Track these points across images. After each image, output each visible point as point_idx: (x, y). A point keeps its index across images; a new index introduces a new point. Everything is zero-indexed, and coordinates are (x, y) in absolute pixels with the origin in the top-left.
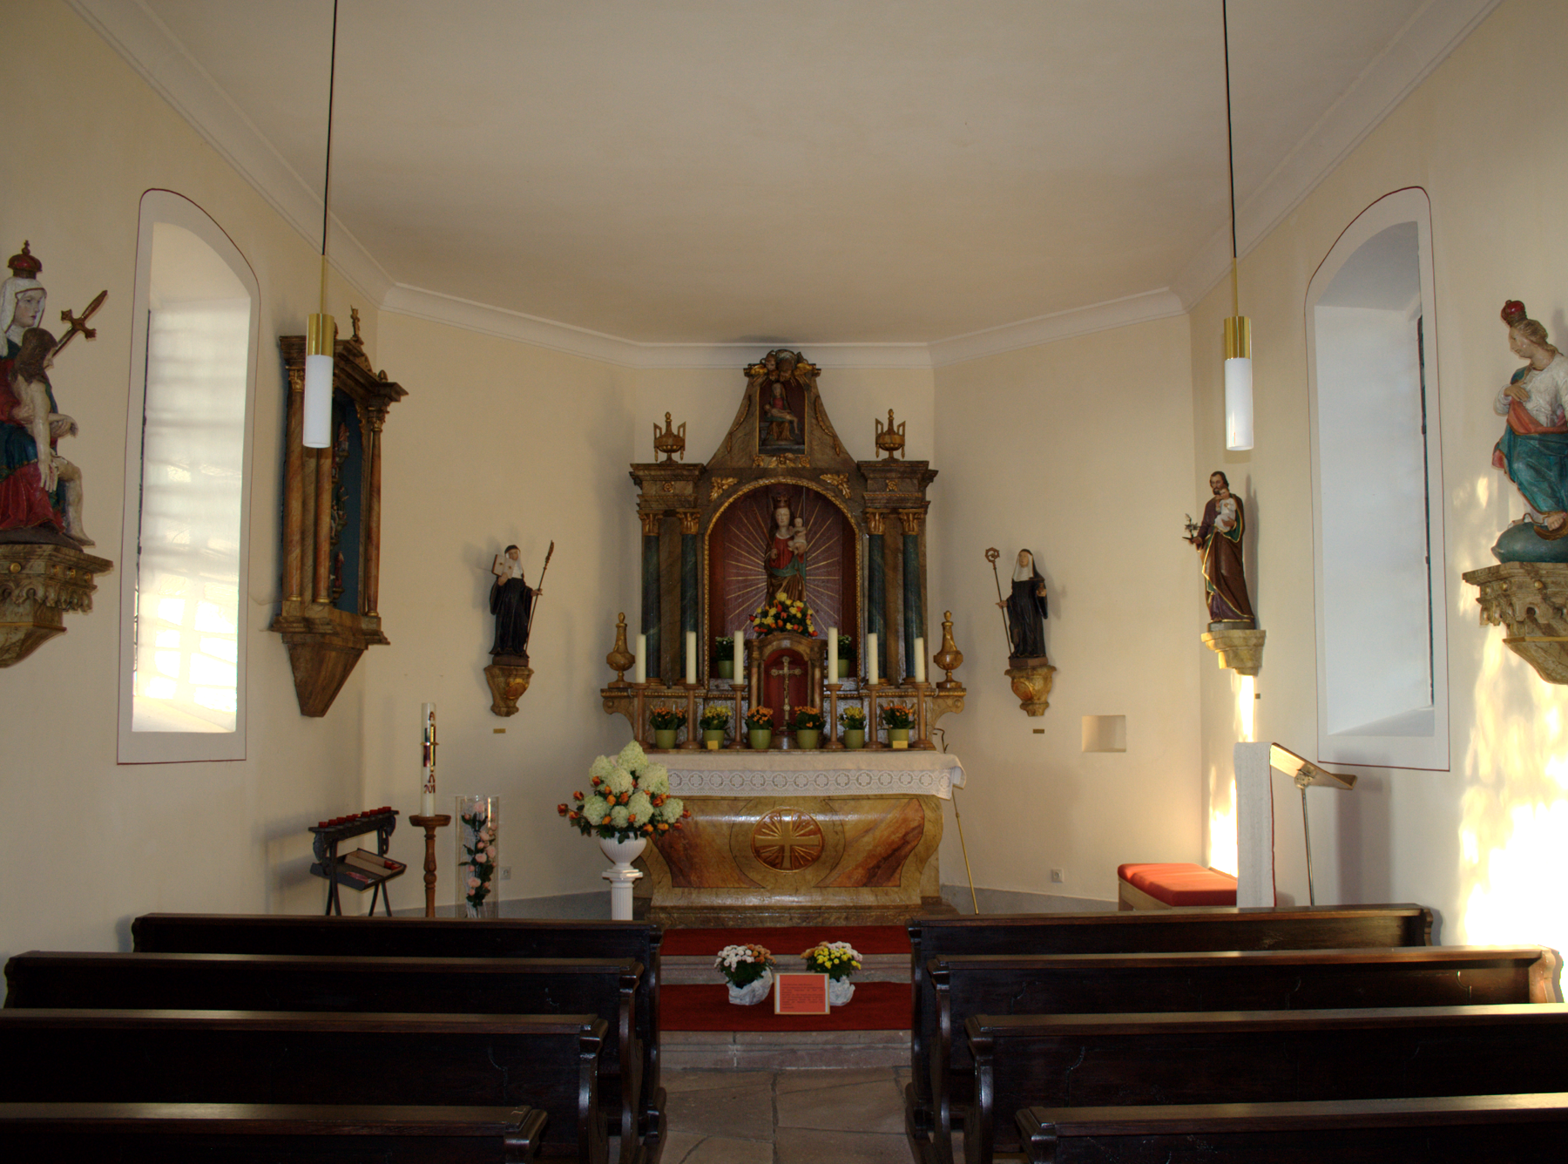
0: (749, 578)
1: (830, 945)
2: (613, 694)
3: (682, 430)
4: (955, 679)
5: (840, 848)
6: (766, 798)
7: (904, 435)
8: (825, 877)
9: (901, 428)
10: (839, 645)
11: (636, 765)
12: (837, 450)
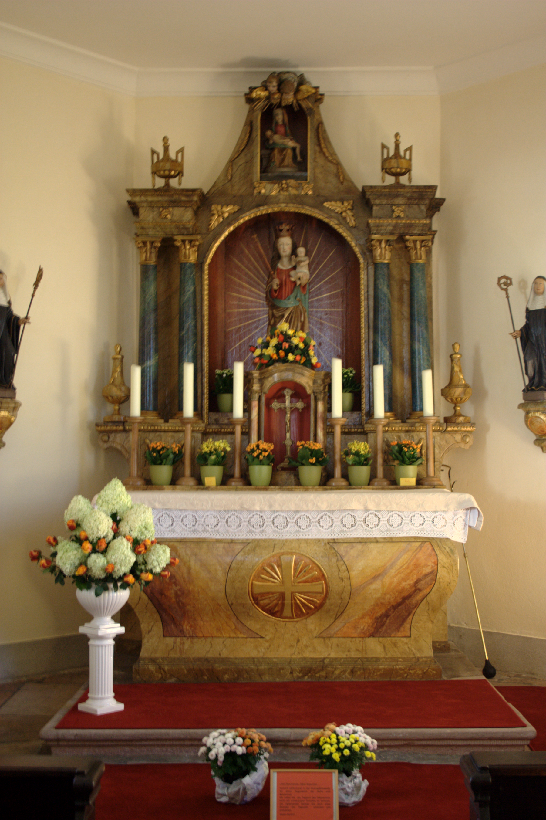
0: (251, 309)
1: (338, 729)
2: (108, 428)
3: (180, 155)
4: (463, 414)
5: (346, 595)
6: (265, 541)
7: (410, 160)
8: (329, 626)
9: (408, 153)
10: (343, 378)
11: (117, 507)
12: (341, 178)
